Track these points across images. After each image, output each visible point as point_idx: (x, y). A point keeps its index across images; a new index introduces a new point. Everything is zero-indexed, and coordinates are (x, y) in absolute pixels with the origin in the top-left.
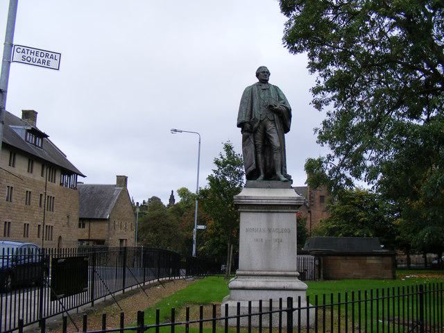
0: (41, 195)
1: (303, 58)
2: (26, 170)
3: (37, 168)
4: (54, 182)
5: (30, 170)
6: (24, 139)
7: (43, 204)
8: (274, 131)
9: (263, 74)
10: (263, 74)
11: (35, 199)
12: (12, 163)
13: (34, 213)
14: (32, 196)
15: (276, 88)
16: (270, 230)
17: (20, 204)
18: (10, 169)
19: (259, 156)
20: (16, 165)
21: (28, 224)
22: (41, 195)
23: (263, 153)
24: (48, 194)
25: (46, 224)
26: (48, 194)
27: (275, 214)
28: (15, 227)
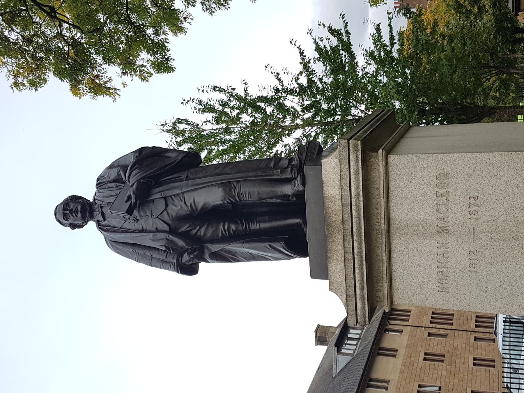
0: (429, 334)
1: (175, 45)
2: (392, 359)
3: (390, 340)
4: (410, 311)
5: (392, 353)
6: (350, 358)
7: (442, 332)
8: (189, 198)
9: (74, 212)
10: (74, 212)
11: (436, 346)
12: (392, 353)
13: (456, 349)
14: (430, 351)
15: (100, 183)
16: (443, 231)
17: (444, 373)
18: (402, 352)
19: (254, 226)
20: (387, 378)
21: (475, 359)
22: (429, 334)
23: (251, 217)
24: (428, 324)
25: (473, 326)
26: (428, 324)
27: (395, 213)
28: (478, 382)
